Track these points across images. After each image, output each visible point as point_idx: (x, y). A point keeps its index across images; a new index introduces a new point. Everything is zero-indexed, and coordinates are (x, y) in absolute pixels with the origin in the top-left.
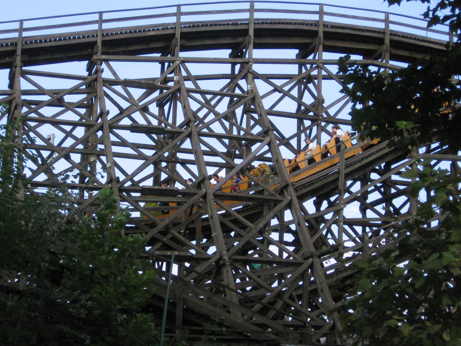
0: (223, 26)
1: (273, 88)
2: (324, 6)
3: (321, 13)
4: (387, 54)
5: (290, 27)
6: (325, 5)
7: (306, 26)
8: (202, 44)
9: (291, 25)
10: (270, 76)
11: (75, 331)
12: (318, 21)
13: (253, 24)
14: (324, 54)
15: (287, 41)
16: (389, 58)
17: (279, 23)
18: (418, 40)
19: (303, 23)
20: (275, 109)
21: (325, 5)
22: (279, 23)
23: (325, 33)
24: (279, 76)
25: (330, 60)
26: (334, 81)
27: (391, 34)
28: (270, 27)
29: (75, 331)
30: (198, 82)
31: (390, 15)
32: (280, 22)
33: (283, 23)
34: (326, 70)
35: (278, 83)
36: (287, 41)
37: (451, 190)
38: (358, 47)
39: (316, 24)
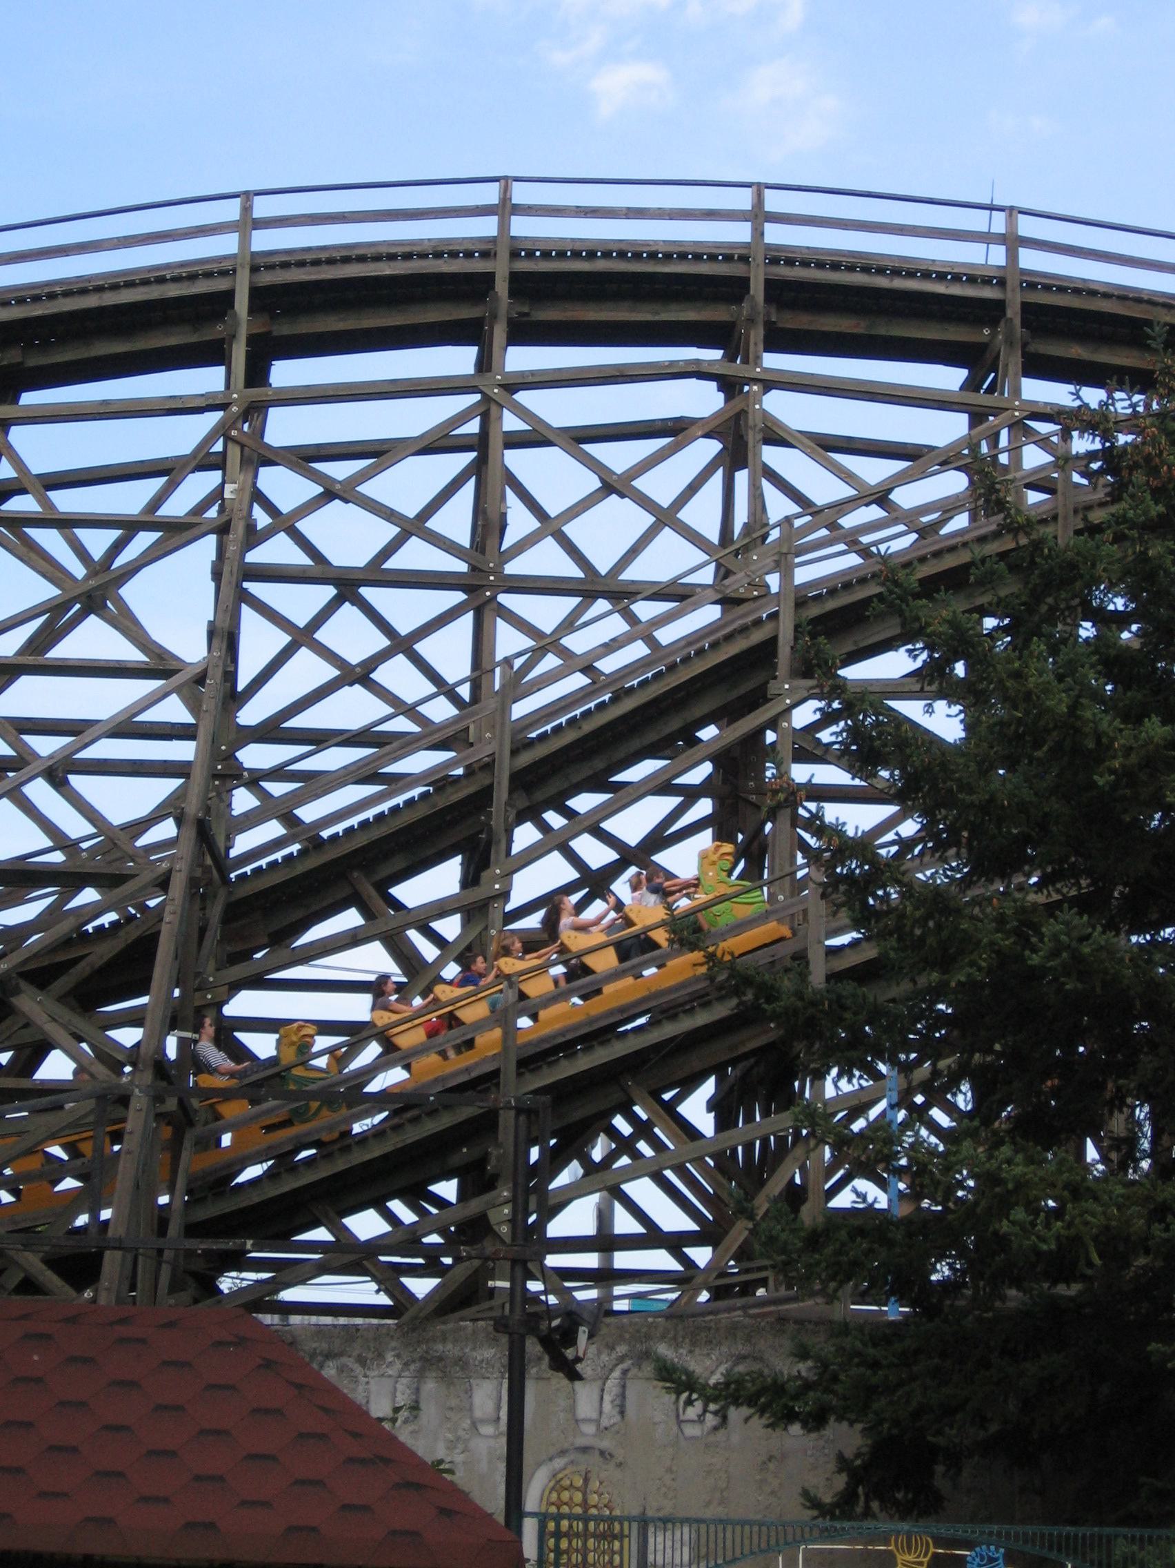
0: (142, 289)
1: (321, 490)
2: (767, 192)
3: (758, 216)
4: (752, 333)
5: (386, 269)
6: (517, 179)
7: (451, 260)
8: (86, 355)
9: (392, 264)
10: (310, 453)
11: (1113, 933)
12: (493, 240)
13: (247, 271)
14: (513, 351)
15: (690, 314)
16: (761, 347)
17: (346, 260)
18: (881, 271)
19: (440, 251)
20: (392, 563)
21: (517, 179)
22: (346, 260)
23: (517, 279)
24: (344, 451)
25: (532, 373)
26: (556, 448)
27: (774, 261)
28: (313, 277)
29: (1113, 933)
30: (52, 495)
31: (516, 186)
32: (348, 255)
33: (362, 259)
34: (522, 412)
35: (340, 470)
36: (690, 314)
37: (971, 795)
38: (665, 316)
39: (487, 250)
